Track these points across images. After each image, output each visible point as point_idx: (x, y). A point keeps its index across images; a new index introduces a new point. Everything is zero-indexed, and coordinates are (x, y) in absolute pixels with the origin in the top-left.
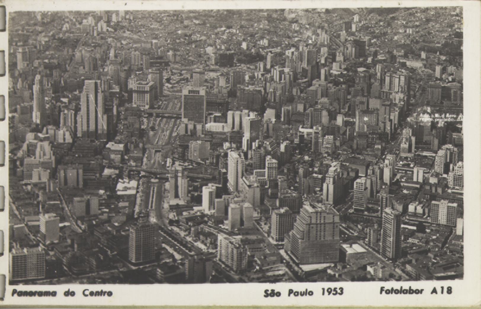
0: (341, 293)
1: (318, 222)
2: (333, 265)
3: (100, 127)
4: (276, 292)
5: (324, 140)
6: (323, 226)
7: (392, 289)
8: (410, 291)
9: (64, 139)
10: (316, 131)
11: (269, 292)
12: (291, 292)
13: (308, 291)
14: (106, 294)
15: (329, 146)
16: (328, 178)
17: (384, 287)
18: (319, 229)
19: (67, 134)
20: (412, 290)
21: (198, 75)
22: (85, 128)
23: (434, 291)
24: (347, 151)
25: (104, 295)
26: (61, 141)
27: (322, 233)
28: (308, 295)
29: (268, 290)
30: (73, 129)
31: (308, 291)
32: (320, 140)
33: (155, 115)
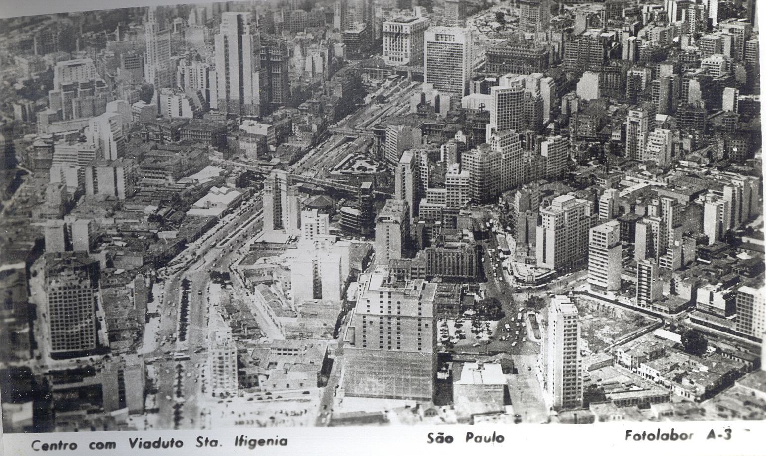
0: (286, 444)
1: (385, 313)
2: (413, 404)
3: (247, 93)
4: (445, 436)
5: (650, 138)
6: (394, 321)
7: (644, 434)
8: (673, 436)
9: (181, 113)
10: (634, 119)
11: (434, 437)
12: (469, 436)
13: (497, 435)
14: (68, 447)
15: (658, 150)
16: (546, 217)
17: (631, 431)
18: (385, 327)
19: (185, 104)
20: (677, 435)
21: (529, 7)
22: (223, 96)
23: (712, 434)
24: (699, 162)
25: (65, 448)
26: (175, 114)
27: (394, 337)
28: (496, 441)
29: (202, 438)
30: (205, 96)
31: (497, 435)
32: (641, 138)
33: (409, 75)
